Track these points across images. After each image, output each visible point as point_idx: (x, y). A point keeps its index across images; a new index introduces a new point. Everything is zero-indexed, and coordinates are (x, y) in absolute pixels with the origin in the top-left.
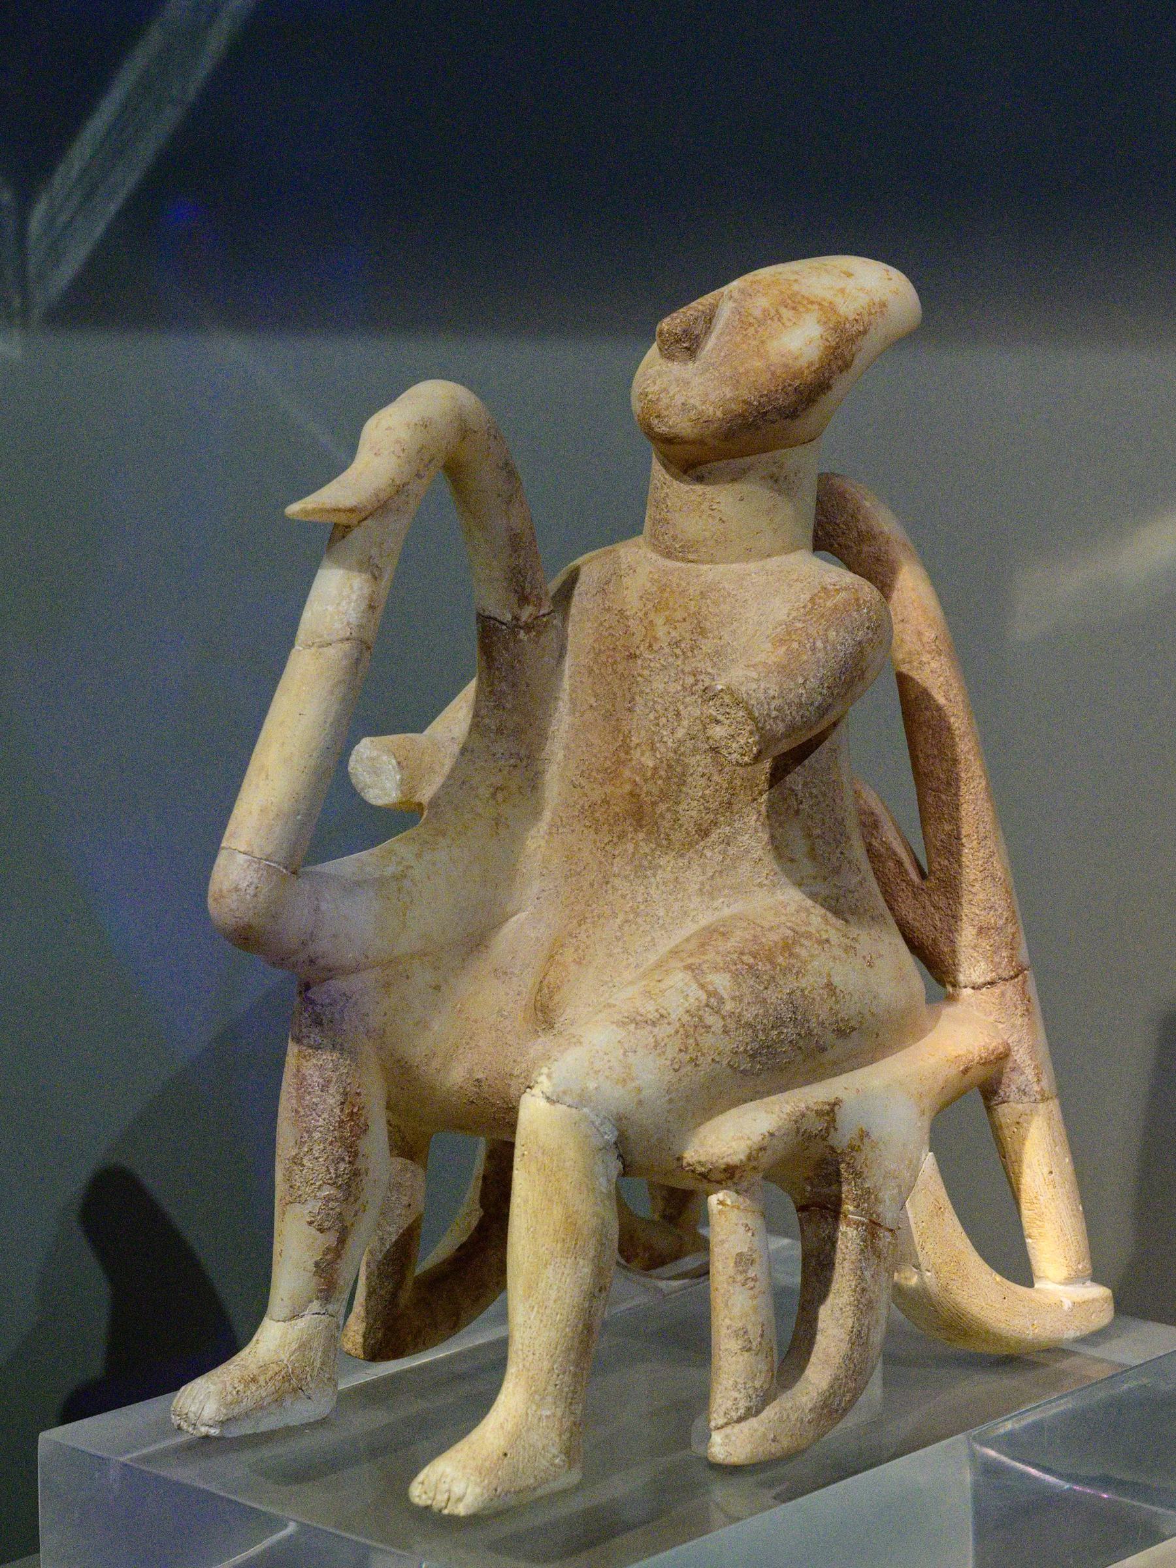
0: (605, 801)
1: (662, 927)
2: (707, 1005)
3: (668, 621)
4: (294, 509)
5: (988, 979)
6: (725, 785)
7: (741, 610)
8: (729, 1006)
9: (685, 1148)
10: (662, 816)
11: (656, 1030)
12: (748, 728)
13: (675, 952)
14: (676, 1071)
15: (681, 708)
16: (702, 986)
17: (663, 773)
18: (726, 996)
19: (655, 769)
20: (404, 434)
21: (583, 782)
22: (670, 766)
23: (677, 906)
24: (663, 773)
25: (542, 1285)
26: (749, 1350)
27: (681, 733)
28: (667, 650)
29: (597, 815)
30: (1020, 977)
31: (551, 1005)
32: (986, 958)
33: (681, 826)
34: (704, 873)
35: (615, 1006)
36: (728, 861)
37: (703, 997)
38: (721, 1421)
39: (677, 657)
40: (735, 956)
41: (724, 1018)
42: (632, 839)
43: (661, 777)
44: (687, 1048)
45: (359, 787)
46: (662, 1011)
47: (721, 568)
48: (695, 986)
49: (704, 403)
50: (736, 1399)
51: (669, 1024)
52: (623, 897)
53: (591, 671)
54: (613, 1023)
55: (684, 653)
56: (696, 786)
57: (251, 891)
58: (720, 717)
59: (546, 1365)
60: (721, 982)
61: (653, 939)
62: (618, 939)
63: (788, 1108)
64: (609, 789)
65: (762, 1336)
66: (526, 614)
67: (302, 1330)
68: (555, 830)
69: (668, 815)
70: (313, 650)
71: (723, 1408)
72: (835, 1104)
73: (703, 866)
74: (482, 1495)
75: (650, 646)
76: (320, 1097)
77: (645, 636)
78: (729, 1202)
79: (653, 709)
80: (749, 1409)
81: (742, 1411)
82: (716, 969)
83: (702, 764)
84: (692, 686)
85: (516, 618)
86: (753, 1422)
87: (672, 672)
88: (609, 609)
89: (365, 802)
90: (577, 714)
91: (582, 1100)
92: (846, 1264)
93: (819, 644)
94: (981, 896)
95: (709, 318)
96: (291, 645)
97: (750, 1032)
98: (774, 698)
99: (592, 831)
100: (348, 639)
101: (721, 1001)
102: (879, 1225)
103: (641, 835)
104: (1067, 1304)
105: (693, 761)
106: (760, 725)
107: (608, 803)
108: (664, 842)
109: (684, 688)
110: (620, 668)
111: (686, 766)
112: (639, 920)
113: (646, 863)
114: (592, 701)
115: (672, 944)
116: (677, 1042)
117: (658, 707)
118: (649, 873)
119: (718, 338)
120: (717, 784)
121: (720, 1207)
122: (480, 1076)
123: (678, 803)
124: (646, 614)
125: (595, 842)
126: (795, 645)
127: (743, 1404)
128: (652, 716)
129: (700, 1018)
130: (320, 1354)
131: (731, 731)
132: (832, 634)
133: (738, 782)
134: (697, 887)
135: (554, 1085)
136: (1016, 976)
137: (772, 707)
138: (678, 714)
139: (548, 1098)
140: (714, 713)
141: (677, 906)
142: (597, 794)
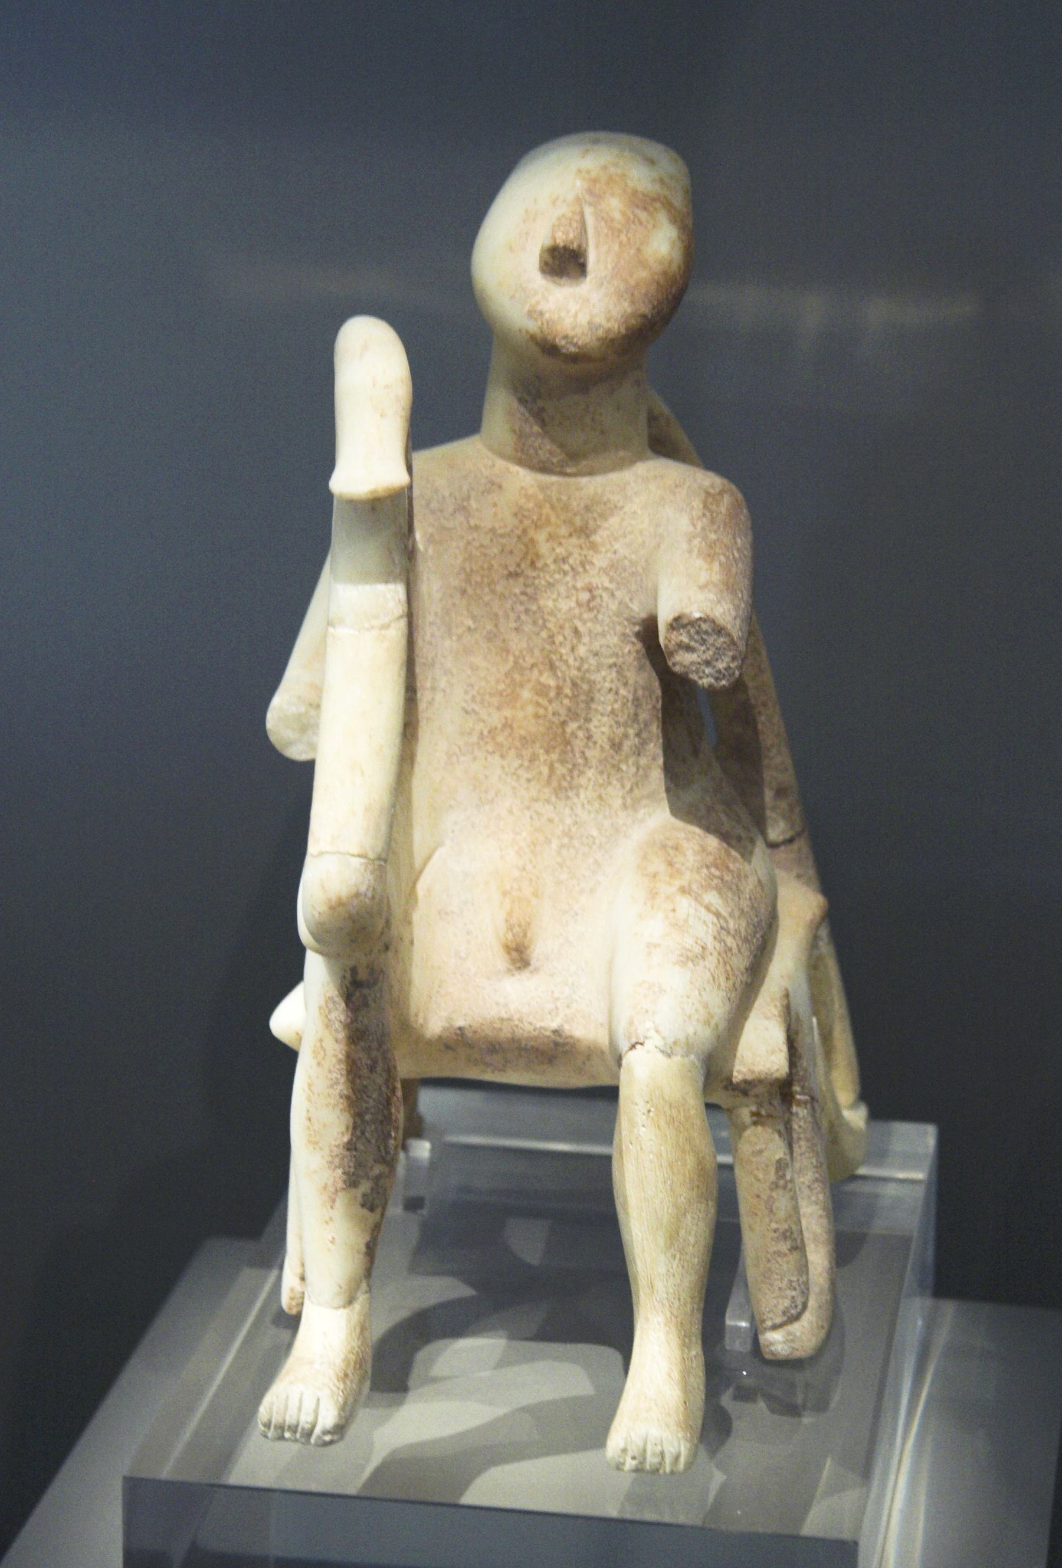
0: (507, 725)
1: (600, 847)
3: (551, 537)
6: (631, 697)
7: (633, 522)
10: (574, 734)
15: (579, 624)
17: (567, 691)
22: (574, 685)
23: (607, 823)
25: (682, 1232)
27: (582, 651)
28: (552, 567)
31: (526, 943)
32: (784, 817)
34: (623, 786)
36: (641, 772)
38: (778, 1320)
39: (565, 573)
42: (545, 761)
43: (567, 696)
47: (599, 480)
48: (703, 911)
49: (608, 320)
50: (793, 1297)
52: (550, 821)
53: (464, 592)
55: (573, 569)
56: (605, 703)
57: (370, 894)
58: (693, 644)
59: (689, 1307)
61: (596, 862)
62: (561, 865)
64: (508, 713)
68: (454, 759)
69: (580, 734)
70: (375, 632)
71: (781, 1308)
73: (621, 780)
75: (533, 564)
76: (369, 1078)
77: (527, 553)
83: (608, 679)
84: (589, 601)
87: (562, 589)
88: (476, 528)
90: (454, 638)
91: (689, 1047)
92: (802, 1143)
99: (497, 757)
103: (555, 756)
105: (597, 677)
107: (511, 727)
109: (579, 604)
110: (499, 588)
111: (592, 683)
112: (576, 843)
113: (565, 784)
114: (470, 622)
118: (570, 794)
119: (597, 247)
120: (624, 697)
121: (755, 1118)
123: (588, 720)
124: (524, 531)
125: (503, 767)
126: (723, 558)
128: (544, 634)
132: (739, 541)
133: (640, 693)
134: (620, 801)
135: (664, 1038)
138: (576, 631)
139: (662, 1052)
141: (607, 823)
142: (495, 719)
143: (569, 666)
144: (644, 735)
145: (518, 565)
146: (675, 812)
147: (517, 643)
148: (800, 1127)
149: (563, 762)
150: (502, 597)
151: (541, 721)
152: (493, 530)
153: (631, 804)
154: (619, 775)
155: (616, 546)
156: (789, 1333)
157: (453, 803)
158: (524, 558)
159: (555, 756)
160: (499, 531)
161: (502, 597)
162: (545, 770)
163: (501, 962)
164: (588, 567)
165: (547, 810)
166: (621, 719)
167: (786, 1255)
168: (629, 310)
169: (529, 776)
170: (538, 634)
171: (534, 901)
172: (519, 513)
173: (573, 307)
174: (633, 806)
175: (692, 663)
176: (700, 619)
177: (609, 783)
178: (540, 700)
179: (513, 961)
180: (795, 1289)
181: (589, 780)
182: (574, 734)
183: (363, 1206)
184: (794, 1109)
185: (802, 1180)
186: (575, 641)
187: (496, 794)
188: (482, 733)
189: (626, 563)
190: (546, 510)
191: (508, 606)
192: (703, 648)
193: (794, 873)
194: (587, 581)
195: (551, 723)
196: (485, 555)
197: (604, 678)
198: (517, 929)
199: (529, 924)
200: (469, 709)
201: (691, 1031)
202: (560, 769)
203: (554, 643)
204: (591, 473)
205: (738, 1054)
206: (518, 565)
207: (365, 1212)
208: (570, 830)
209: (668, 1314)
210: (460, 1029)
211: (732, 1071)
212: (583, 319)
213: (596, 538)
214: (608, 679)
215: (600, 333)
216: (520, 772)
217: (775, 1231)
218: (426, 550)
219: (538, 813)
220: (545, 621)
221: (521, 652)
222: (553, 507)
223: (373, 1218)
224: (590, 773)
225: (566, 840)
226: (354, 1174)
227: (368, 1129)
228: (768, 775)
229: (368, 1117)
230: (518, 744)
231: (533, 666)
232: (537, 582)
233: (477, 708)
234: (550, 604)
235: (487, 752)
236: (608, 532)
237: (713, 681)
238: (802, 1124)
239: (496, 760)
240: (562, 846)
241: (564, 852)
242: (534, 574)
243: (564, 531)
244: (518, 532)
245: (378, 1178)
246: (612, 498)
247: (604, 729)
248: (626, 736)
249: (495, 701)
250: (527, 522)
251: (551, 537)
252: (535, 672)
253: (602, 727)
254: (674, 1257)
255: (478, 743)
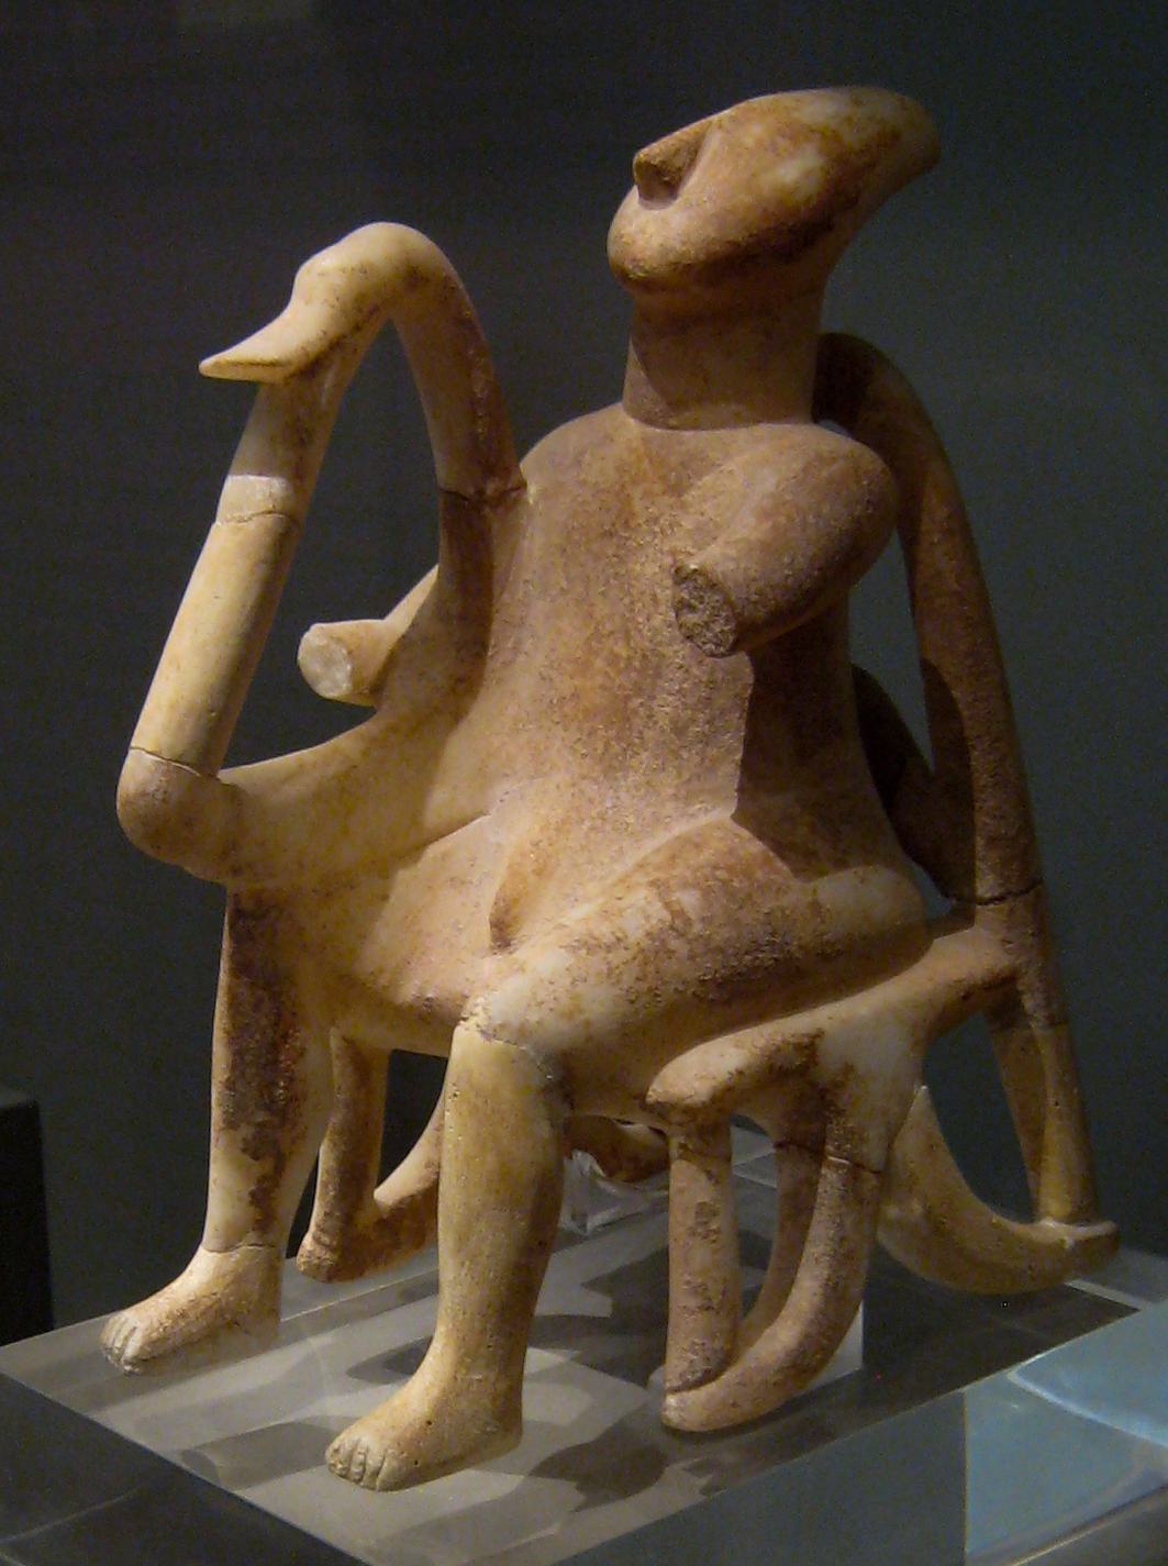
0: (575, 696)
2: (672, 928)
3: (646, 494)
4: (207, 365)
5: (996, 894)
8: (697, 928)
9: (650, 1082)
10: (635, 712)
11: (610, 956)
12: (724, 614)
13: (641, 866)
14: (632, 1002)
16: (667, 905)
17: (637, 664)
18: (693, 917)
19: (629, 659)
20: (339, 281)
21: (554, 674)
22: (644, 656)
24: (637, 664)
26: (708, 1308)
29: (566, 709)
30: (1032, 892)
33: (656, 723)
34: (679, 775)
35: (565, 926)
37: (667, 916)
38: (676, 1383)
39: (655, 534)
40: (707, 871)
41: (689, 942)
43: (635, 670)
44: (645, 976)
45: (309, 680)
46: (619, 935)
47: (704, 434)
48: (659, 905)
49: (684, 243)
51: (626, 949)
52: (591, 801)
54: (561, 947)
60: (689, 900)
62: (583, 848)
63: (761, 1042)
65: (724, 1293)
66: (491, 488)
67: (237, 1262)
70: (233, 524)
71: (680, 1370)
72: (819, 1034)
74: (400, 1469)
75: (626, 522)
78: (690, 1147)
79: (628, 593)
80: (707, 1372)
81: (699, 1374)
82: (685, 885)
83: (680, 654)
85: (481, 492)
86: (711, 1387)
89: (316, 695)
91: (522, 1033)
93: (811, 519)
94: (991, 803)
95: (694, 150)
96: (212, 518)
97: (720, 957)
98: (754, 580)
100: (270, 512)
101: (688, 922)
102: (863, 1167)
103: (612, 733)
104: (1069, 1242)
105: (668, 651)
106: (738, 611)
107: (578, 697)
108: (637, 741)
112: (608, 827)
113: (616, 764)
114: (564, 584)
115: (641, 855)
116: (635, 970)
117: (634, 591)
118: (619, 774)
120: (696, 677)
121: (681, 1151)
122: (430, 995)
123: (653, 698)
127: (701, 1366)
128: (627, 601)
129: (663, 941)
130: (257, 1287)
131: (705, 618)
136: (1027, 891)
137: (753, 589)
139: (483, 1032)
140: (687, 597)
141: (648, 812)
143: (642, 637)
144: (718, 723)
145: (613, 525)
146: (741, 817)
147: (601, 609)
148: (826, 1192)
149: (618, 739)
150: (597, 558)
151: (606, 693)
152: (596, 483)
153: (686, 797)
154: (676, 763)
155: (705, 507)
156: (682, 1401)
157: (508, 771)
158: (618, 517)
159: (612, 733)
160: (602, 486)
161: (597, 558)
162: (600, 747)
163: (484, 932)
164: (675, 529)
165: (591, 789)
166: (690, 700)
167: (693, 1312)
168: (713, 235)
169: (584, 751)
170: (622, 599)
171: (532, 879)
172: (621, 469)
173: (651, 229)
174: (686, 798)
175: (695, 624)
176: (695, 570)
177: (664, 769)
178: (608, 669)
179: (495, 939)
180: (697, 1354)
181: (641, 763)
182: (635, 712)
183: (244, 1151)
184: (823, 1171)
185: (812, 1250)
186: (652, 609)
187: (551, 768)
188: (551, 702)
189: (711, 525)
190: (645, 464)
191: (600, 568)
192: (701, 606)
193: (999, 936)
194: (674, 544)
195: (616, 696)
196: (586, 512)
197: (676, 652)
198: (502, 904)
199: (516, 901)
200: (545, 674)
201: (533, 1017)
202: (616, 748)
203: (632, 610)
204: (696, 427)
205: (661, 1074)
206: (613, 525)
207: (247, 1159)
208: (606, 812)
209: (451, 1326)
210: (428, 999)
211: (648, 1089)
212: (656, 242)
213: (687, 497)
214: (680, 654)
215: (671, 257)
216: (578, 746)
217: (688, 1283)
218: (536, 503)
219: (582, 792)
220: (631, 586)
221: (602, 617)
222: (651, 462)
223: (258, 1168)
224: (644, 755)
225: (599, 822)
226: (233, 1114)
227: (248, 1070)
228: (981, 819)
229: (248, 1058)
230: (581, 717)
231: (612, 633)
232: (628, 543)
233: (554, 674)
234: (638, 567)
235: (553, 721)
236: (700, 492)
237: (713, 647)
238: (828, 1188)
239: (559, 731)
240: (593, 828)
241: (592, 835)
242: (627, 535)
243: (658, 488)
244: (617, 488)
245: (261, 1125)
246: (710, 454)
247: (667, 709)
248: (693, 721)
249: (569, 668)
250: (627, 478)
251: (646, 494)
252: (611, 641)
253: (666, 706)
254: (463, 1264)
255: (546, 713)
